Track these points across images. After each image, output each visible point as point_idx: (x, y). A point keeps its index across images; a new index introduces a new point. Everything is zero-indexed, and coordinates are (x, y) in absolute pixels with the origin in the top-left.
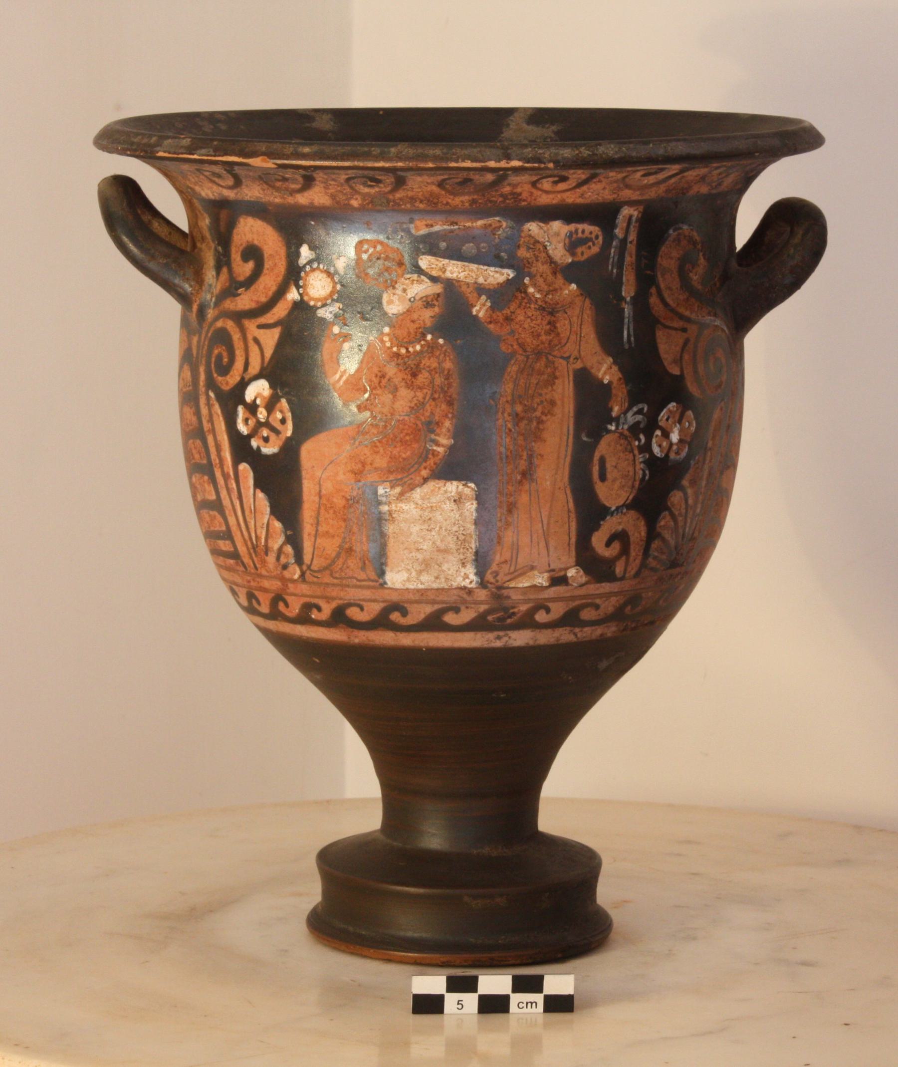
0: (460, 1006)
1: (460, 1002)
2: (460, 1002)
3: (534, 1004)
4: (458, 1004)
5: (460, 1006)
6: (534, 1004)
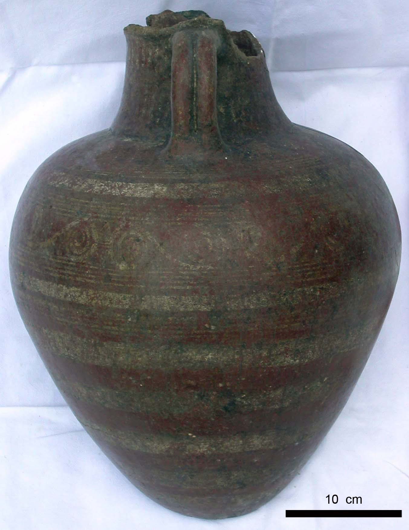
0: (349, 500)
3: (359, 499)
6: (359, 499)
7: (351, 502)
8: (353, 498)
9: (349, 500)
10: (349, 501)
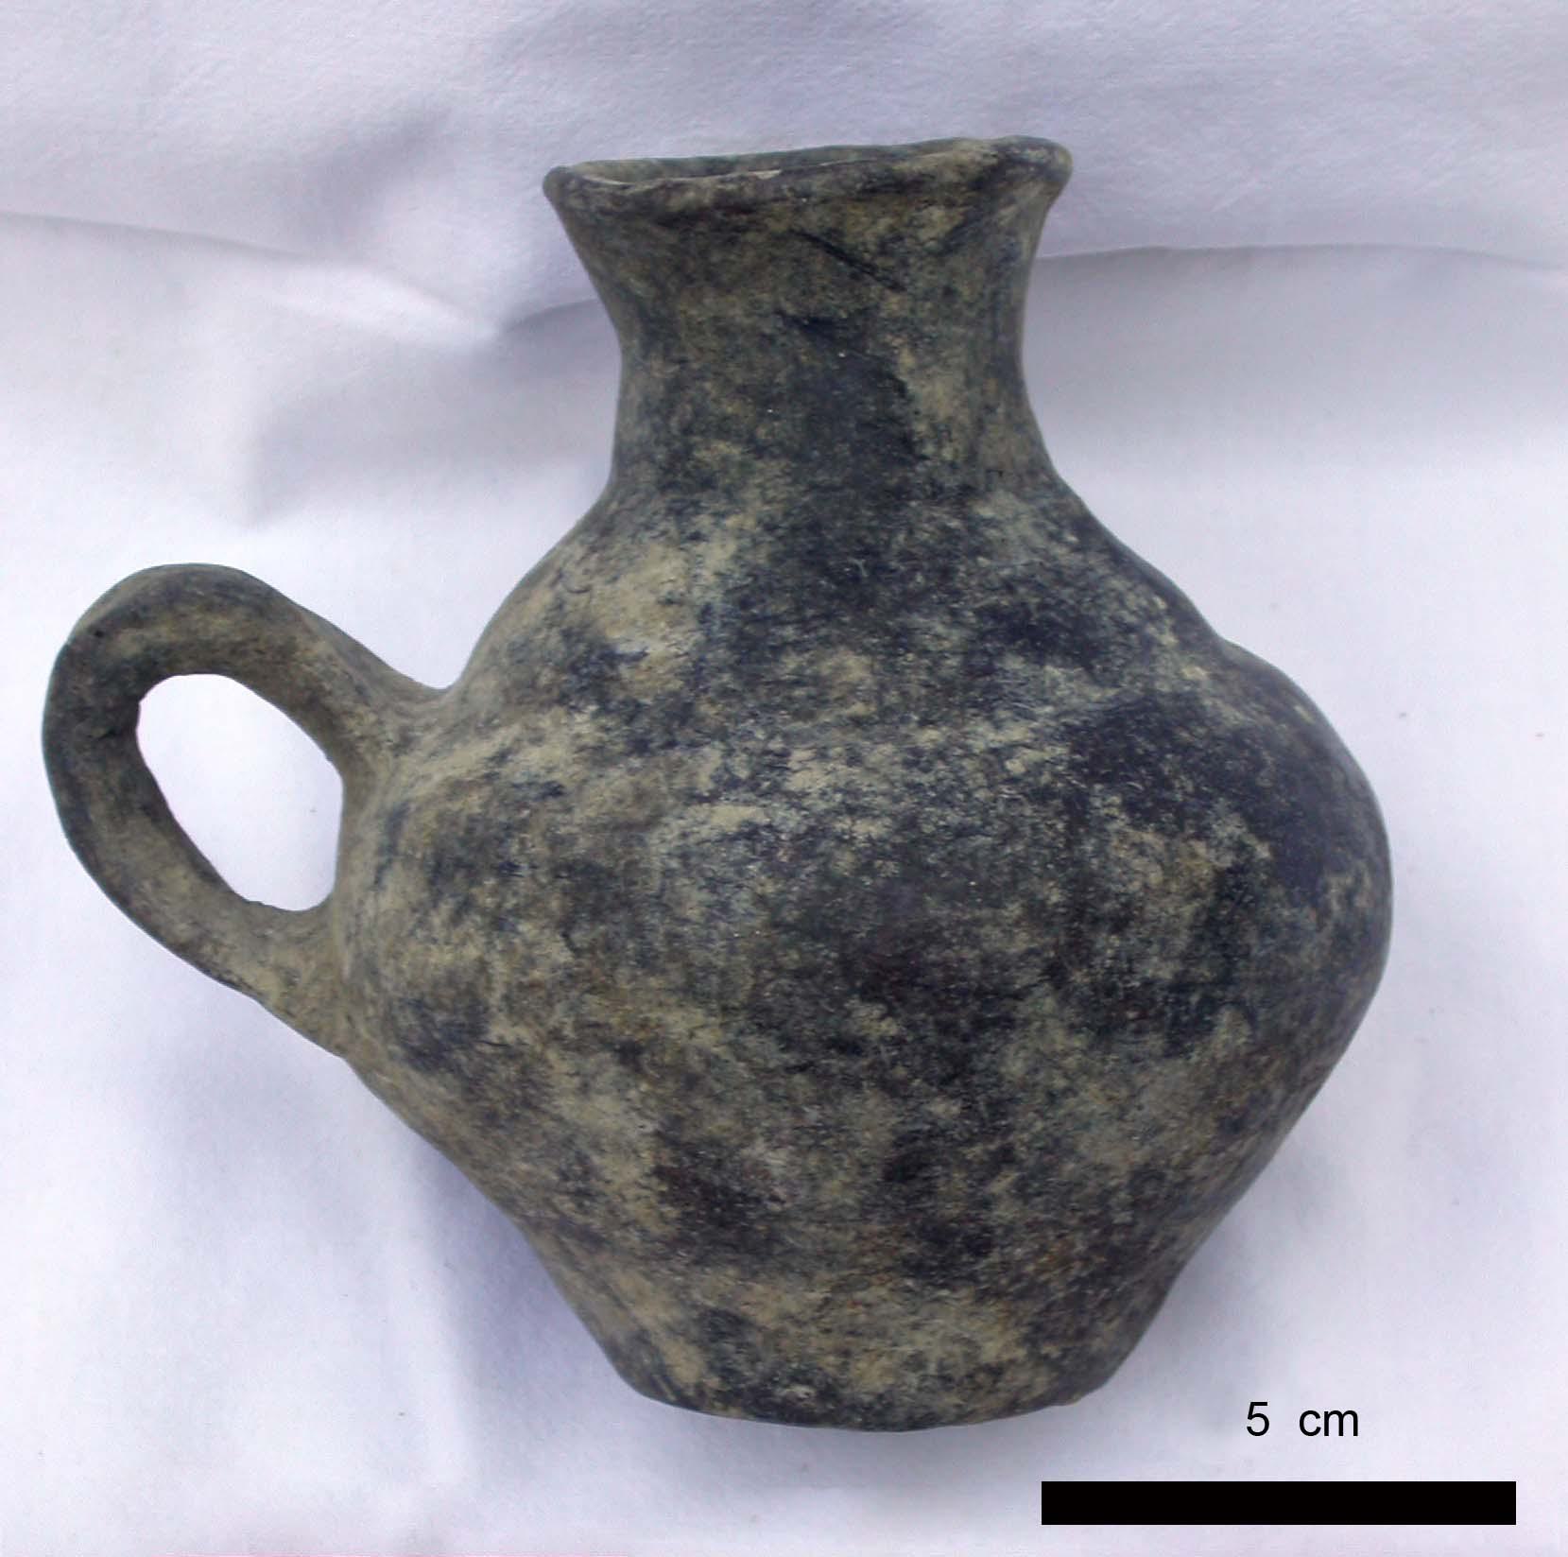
0: (1311, 1423)
1: (1257, 1410)
2: (1257, 1410)
3: (1348, 1420)
4: (1251, 1416)
5: (1258, 1425)
6: (1348, 1420)
7: (1318, 1429)
8: (1327, 1416)
9: (1311, 1423)
10: (1310, 1427)
